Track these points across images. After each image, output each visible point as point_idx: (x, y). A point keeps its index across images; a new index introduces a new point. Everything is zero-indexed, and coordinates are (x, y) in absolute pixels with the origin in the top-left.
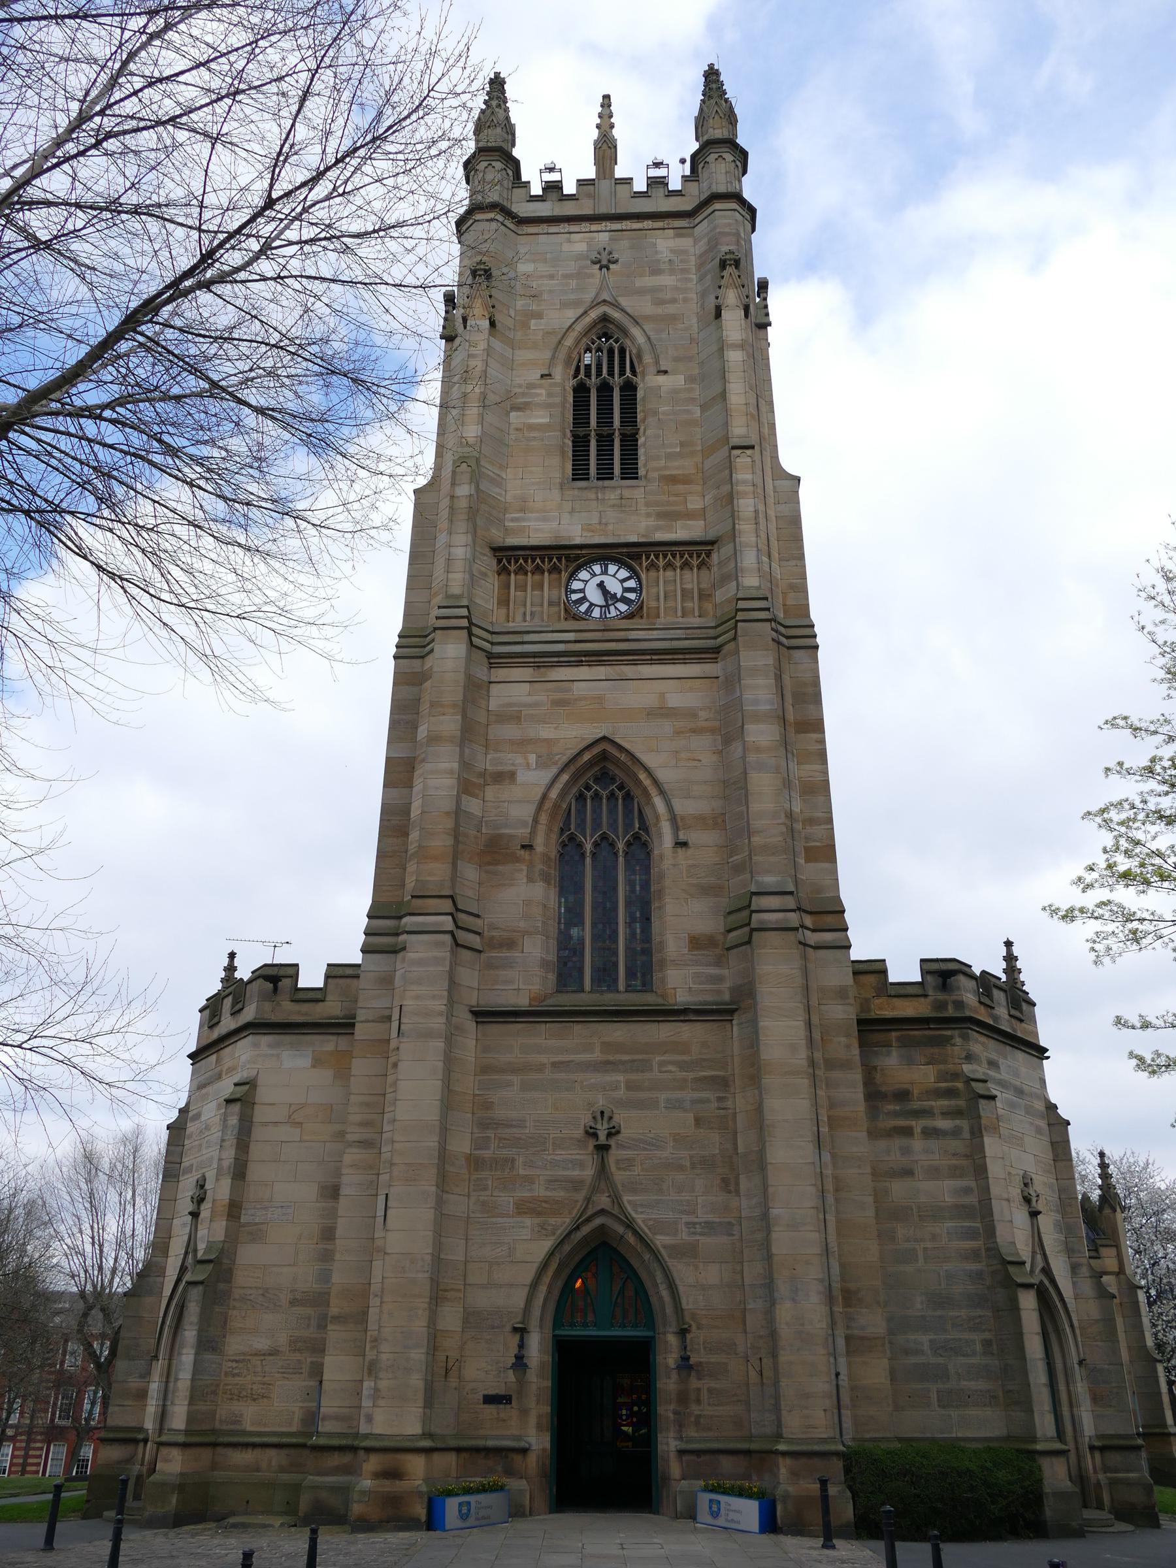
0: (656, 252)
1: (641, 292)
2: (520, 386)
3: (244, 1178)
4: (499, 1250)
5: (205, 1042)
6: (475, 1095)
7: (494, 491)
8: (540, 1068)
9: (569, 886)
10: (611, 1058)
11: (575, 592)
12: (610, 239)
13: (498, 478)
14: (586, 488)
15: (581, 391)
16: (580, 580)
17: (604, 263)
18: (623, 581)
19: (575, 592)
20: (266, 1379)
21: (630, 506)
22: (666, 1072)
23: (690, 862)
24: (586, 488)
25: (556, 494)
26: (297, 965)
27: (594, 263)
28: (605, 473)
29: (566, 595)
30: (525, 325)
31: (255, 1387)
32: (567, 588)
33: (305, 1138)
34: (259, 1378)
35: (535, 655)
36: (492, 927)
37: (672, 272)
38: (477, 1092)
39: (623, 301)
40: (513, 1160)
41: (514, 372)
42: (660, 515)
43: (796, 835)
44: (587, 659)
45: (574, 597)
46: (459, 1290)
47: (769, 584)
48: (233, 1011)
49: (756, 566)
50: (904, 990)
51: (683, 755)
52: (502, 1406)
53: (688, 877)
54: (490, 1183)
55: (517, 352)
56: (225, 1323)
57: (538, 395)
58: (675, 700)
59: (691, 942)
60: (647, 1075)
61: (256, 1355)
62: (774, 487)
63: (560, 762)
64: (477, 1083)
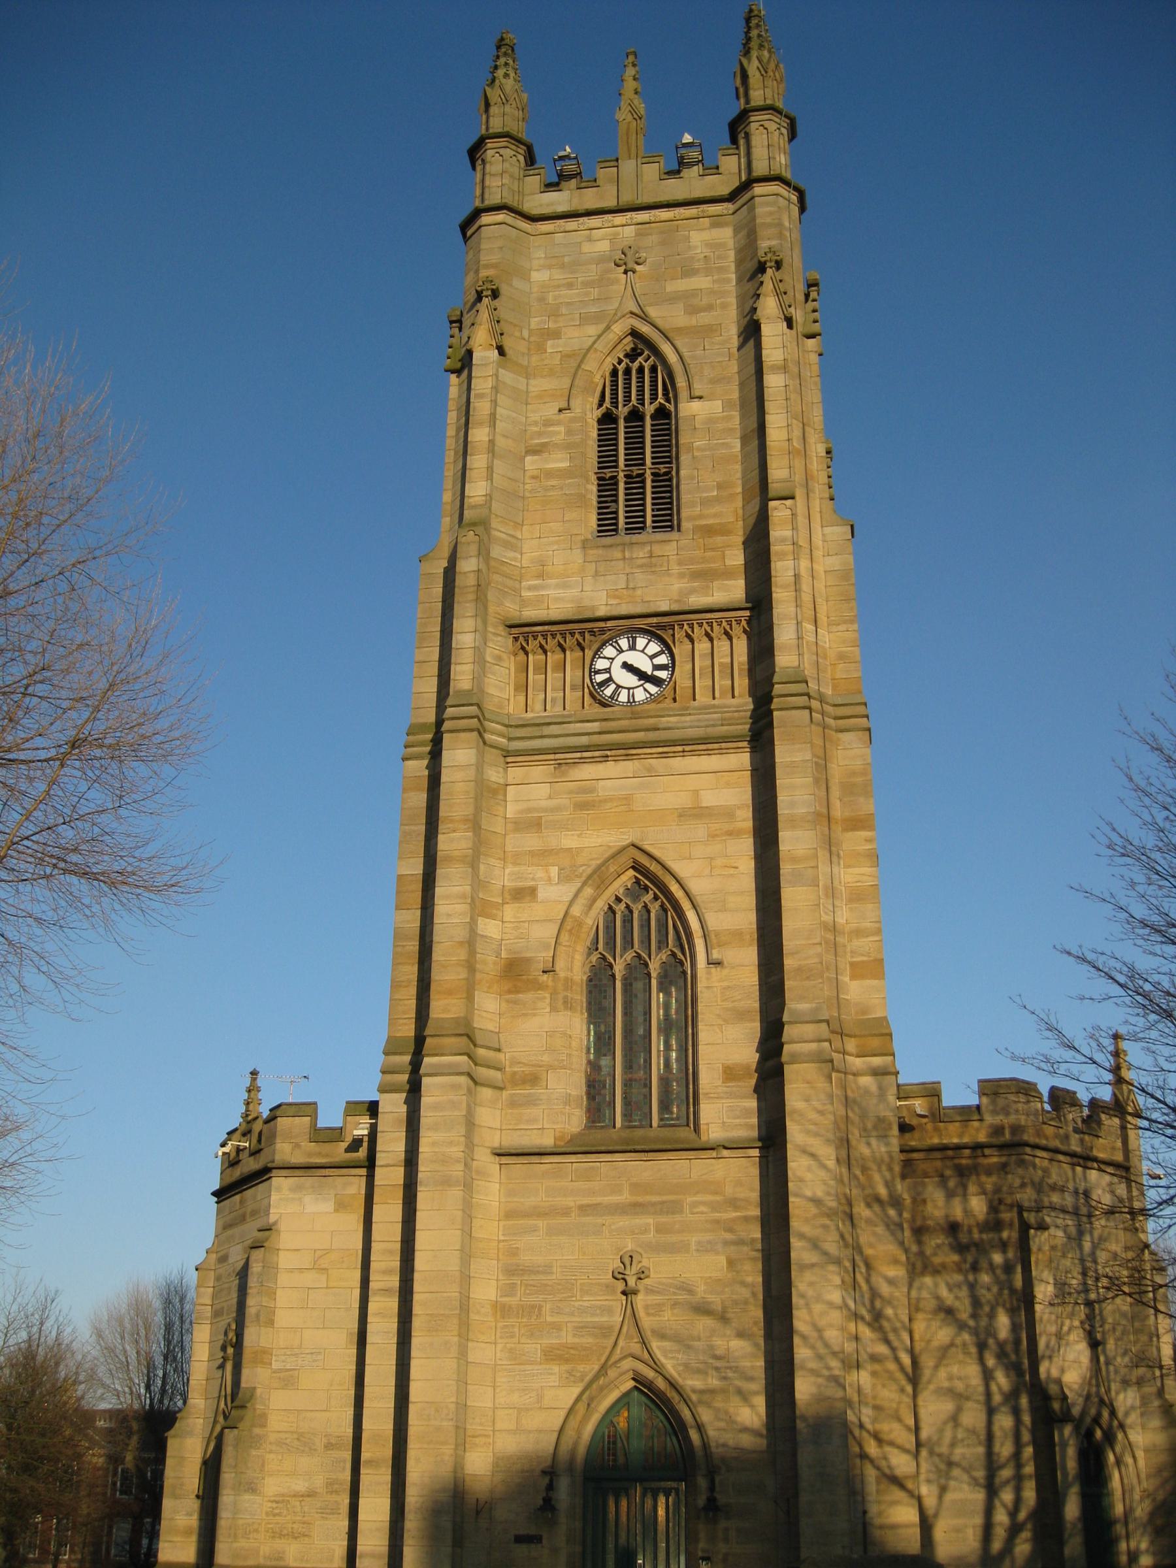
0: (690, 247)
1: (673, 299)
2: (536, 423)
3: (273, 1324)
4: (527, 1397)
5: (229, 1180)
6: (499, 1241)
7: (509, 555)
8: (566, 1212)
9: (598, 1010)
10: (640, 1199)
11: (598, 672)
12: (637, 235)
13: (513, 540)
14: (611, 546)
15: (607, 419)
16: (605, 658)
17: (626, 262)
18: (652, 657)
19: (598, 672)
20: (305, 1519)
21: (661, 566)
22: (697, 1213)
23: (726, 984)
24: (611, 546)
25: (577, 556)
26: (315, 1103)
27: (617, 265)
28: (636, 525)
29: (590, 676)
30: (541, 349)
31: (295, 1526)
32: (591, 668)
33: (331, 1284)
34: (298, 1518)
35: (555, 751)
36: (515, 1062)
37: (708, 272)
38: (502, 1238)
39: (652, 312)
40: (540, 1307)
41: (529, 407)
42: (697, 575)
43: (840, 950)
44: (613, 753)
45: (599, 678)
46: (487, 1436)
47: (815, 657)
48: (267, 1233)
49: (795, 642)
50: (967, 1114)
51: (719, 862)
52: (533, 1546)
53: (723, 1001)
54: (516, 1330)
55: (532, 382)
56: (263, 1465)
57: (559, 433)
58: (709, 799)
59: (724, 1072)
60: (678, 1217)
61: (294, 1496)
62: (823, 535)
63: (584, 874)
64: (501, 1228)
